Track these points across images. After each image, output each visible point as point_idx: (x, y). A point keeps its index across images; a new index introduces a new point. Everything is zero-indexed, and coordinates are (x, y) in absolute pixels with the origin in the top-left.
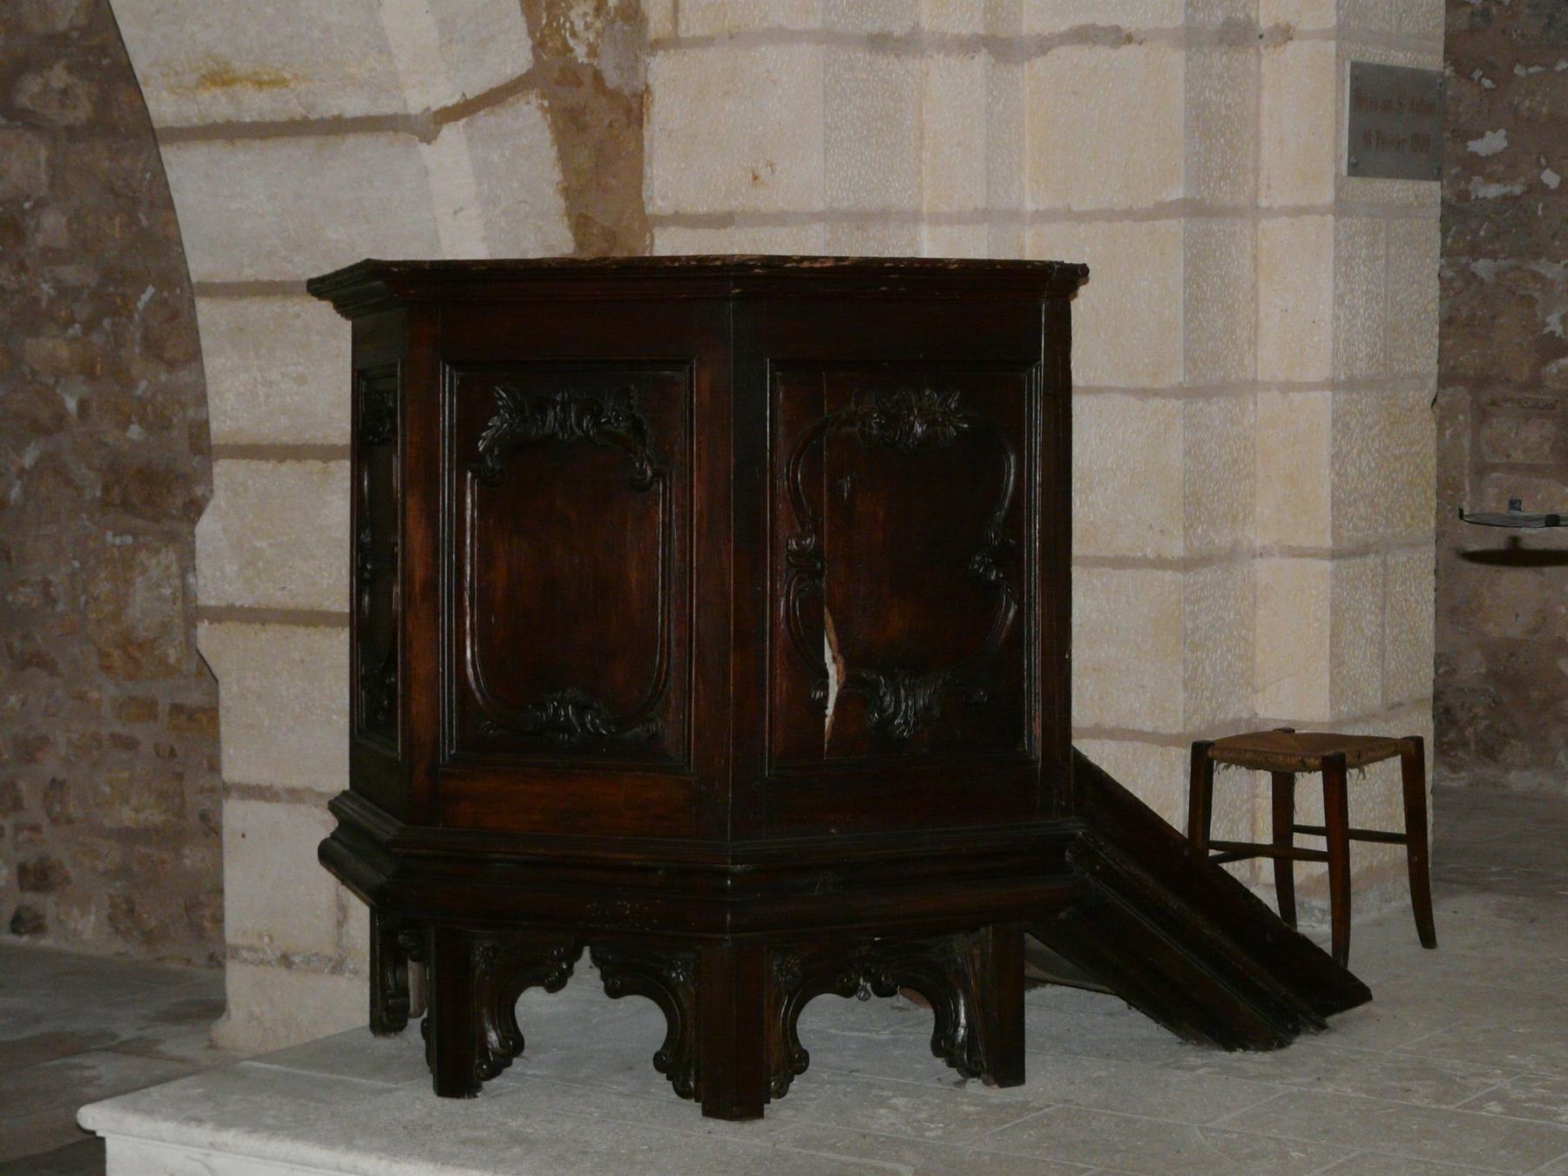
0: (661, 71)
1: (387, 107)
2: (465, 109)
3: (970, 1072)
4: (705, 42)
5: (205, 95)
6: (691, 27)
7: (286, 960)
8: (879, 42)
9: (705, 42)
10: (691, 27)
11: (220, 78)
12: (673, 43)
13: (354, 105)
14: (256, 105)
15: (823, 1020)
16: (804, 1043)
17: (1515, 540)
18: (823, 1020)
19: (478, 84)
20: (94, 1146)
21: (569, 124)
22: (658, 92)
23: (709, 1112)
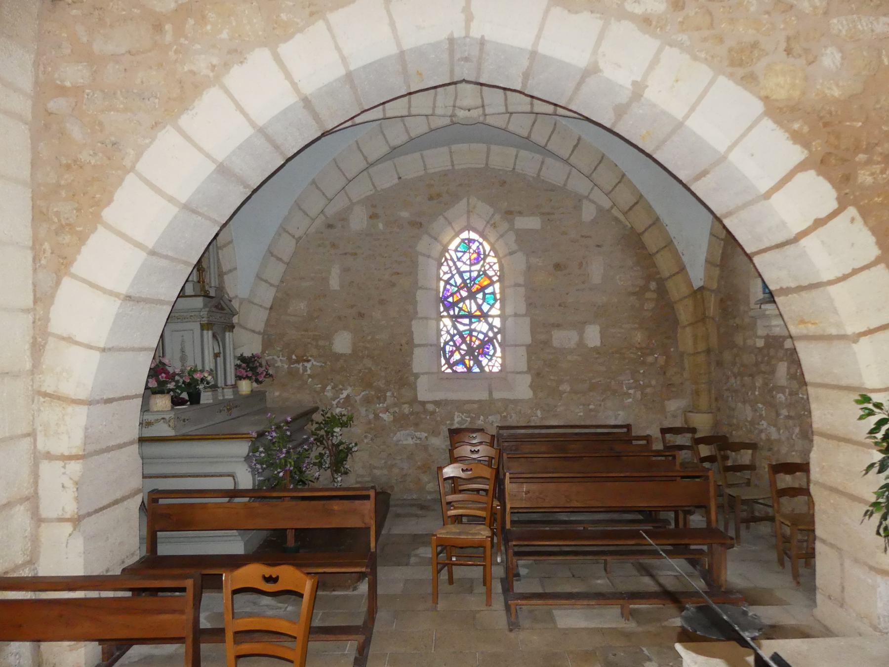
1: (842, 332)
5: (802, 326)
7: (829, 597)
13: (833, 331)
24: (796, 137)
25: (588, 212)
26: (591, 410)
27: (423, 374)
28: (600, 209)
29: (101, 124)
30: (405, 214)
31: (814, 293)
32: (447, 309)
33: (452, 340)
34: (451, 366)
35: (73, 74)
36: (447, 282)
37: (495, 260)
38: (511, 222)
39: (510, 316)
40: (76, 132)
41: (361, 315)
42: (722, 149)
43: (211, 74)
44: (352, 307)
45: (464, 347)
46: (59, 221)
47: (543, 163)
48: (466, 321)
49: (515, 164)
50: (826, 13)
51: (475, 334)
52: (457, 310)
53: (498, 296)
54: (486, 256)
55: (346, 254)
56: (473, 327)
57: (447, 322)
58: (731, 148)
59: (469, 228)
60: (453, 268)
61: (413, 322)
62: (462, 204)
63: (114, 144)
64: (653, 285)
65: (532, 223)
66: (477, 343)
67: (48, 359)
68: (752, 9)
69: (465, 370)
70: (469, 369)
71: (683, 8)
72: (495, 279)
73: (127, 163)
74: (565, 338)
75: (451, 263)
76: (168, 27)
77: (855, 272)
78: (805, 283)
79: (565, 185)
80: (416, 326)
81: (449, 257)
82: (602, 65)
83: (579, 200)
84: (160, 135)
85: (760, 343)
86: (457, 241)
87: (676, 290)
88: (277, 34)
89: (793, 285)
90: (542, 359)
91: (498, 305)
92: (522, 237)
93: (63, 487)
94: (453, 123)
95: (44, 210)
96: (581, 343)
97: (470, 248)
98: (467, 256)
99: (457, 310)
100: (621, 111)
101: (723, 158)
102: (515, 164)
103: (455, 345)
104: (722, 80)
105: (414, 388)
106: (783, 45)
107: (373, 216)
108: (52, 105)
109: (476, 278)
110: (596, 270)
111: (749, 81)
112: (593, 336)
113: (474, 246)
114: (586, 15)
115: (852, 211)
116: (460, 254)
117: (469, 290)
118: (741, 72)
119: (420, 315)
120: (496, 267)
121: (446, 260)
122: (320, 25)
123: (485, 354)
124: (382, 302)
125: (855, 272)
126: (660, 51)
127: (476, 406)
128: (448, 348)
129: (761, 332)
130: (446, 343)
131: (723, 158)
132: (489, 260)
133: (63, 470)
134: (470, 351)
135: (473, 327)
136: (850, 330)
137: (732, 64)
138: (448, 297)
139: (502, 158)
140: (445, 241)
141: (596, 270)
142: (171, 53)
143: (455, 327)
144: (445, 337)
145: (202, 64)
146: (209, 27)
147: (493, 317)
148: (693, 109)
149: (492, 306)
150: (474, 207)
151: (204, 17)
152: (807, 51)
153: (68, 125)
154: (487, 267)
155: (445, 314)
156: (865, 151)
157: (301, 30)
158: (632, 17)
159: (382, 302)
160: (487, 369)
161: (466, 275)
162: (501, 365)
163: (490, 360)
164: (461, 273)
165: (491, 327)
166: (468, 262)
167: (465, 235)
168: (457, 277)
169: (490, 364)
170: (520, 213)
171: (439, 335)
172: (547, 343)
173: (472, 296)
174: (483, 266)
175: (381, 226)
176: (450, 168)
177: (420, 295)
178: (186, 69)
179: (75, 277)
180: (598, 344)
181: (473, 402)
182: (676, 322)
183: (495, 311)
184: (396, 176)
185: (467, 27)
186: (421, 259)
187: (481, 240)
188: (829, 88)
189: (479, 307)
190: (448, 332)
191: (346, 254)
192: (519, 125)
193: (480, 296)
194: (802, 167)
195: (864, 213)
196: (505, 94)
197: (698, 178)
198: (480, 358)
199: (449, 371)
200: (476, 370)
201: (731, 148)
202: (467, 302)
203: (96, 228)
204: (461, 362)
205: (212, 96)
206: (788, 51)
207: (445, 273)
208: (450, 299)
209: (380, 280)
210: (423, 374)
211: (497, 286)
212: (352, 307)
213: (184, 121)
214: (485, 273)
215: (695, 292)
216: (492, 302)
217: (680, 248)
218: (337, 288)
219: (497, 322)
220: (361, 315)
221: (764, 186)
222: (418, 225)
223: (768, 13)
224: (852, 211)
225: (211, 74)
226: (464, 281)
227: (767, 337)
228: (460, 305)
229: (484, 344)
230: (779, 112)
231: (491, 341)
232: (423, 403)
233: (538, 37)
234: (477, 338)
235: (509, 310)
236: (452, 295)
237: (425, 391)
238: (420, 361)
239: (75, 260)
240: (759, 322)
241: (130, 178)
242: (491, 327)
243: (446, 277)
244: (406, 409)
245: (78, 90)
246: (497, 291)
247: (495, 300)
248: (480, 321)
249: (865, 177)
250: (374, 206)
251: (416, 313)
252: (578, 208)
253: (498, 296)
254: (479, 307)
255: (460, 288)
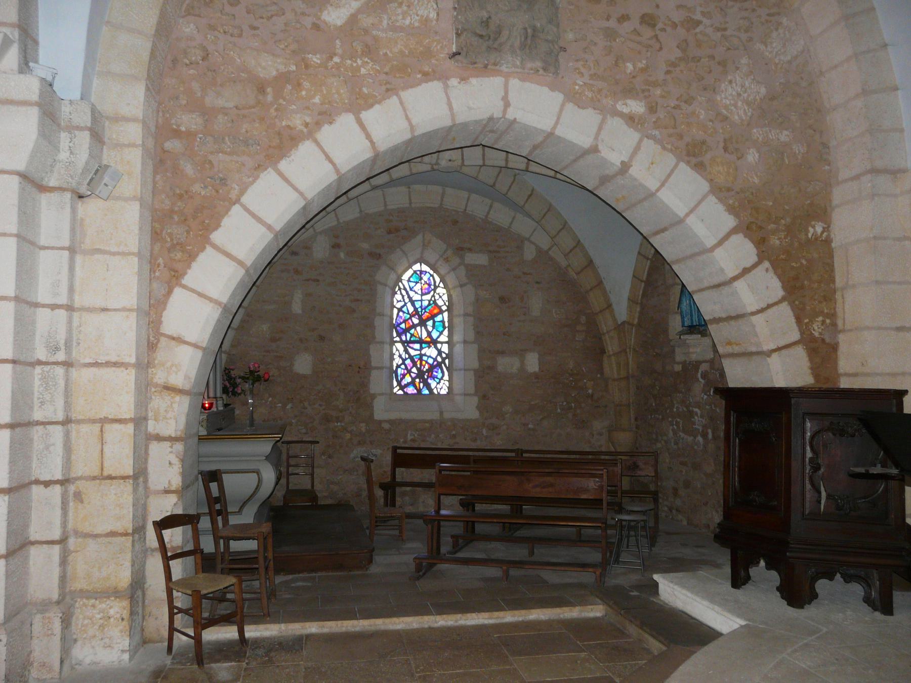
0: (841, 338)
1: (760, 350)
2: (779, 349)
3: (875, 609)
4: (851, 330)
5: (727, 347)
6: (848, 327)
8: (899, 329)
9: (851, 330)
10: (848, 327)
11: (729, 343)
12: (843, 331)
13: (754, 349)
14: (736, 349)
15: (822, 586)
16: (817, 590)
17: (867, 471)
18: (822, 586)
19: (782, 343)
20: (656, 585)
21: (812, 352)
22: (841, 344)
23: (789, 604)
24: (731, 210)
25: (529, 253)
26: (529, 429)
27: (380, 394)
28: (539, 251)
29: (210, 162)
30: (365, 246)
31: (740, 321)
32: (399, 335)
33: (403, 363)
34: (402, 388)
35: (189, 121)
36: (400, 310)
37: (444, 291)
38: (462, 258)
39: (458, 342)
40: (189, 169)
41: (322, 338)
42: (681, 214)
43: (305, 130)
44: (313, 330)
45: (414, 370)
46: (172, 240)
47: (491, 206)
48: (417, 346)
49: (466, 206)
50: (748, 125)
51: (425, 358)
52: (409, 335)
53: (447, 325)
54: (436, 287)
55: (308, 280)
56: (423, 352)
57: (400, 346)
58: (687, 215)
59: (421, 261)
60: (406, 297)
61: (371, 346)
62: (419, 238)
63: (221, 179)
64: (583, 319)
65: (481, 259)
66: (427, 367)
67: (160, 355)
68: (702, 117)
69: (415, 391)
70: (419, 391)
71: (656, 112)
72: (444, 308)
73: (233, 195)
74: (507, 364)
75: (404, 292)
76: (269, 90)
77: (769, 306)
78: (733, 314)
79: (510, 227)
80: (373, 350)
81: (402, 287)
82: (600, 147)
83: (520, 242)
84: (262, 175)
85: (678, 368)
86: (410, 272)
87: (605, 324)
88: (359, 103)
89: (724, 315)
90: (485, 380)
91: (446, 332)
92: (471, 270)
93: (170, 463)
94: (433, 170)
95: (159, 231)
96: (522, 369)
97: (421, 279)
98: (419, 286)
99: (409, 335)
100: (605, 180)
101: (681, 221)
102: (466, 206)
103: (406, 368)
104: (682, 165)
105: (370, 407)
106: (722, 145)
107: (336, 246)
108: (168, 145)
109: (426, 307)
110: (536, 303)
111: (699, 167)
112: (532, 363)
113: (425, 278)
114: (590, 111)
115: (766, 264)
116: (412, 284)
117: (420, 318)
118: (694, 160)
119: (377, 340)
120: (445, 298)
121: (400, 289)
122: (394, 99)
123: (434, 378)
124: (341, 326)
125: (769, 306)
126: (641, 141)
127: (427, 425)
128: (400, 371)
129: (679, 357)
130: (398, 366)
131: (681, 221)
132: (439, 290)
133: (170, 449)
134: (420, 374)
135: (423, 352)
136: (766, 348)
137: (688, 155)
138: (401, 323)
139: (455, 200)
140: (400, 271)
141: (536, 303)
142: (272, 111)
143: (406, 351)
144: (397, 361)
145: (297, 121)
146: (304, 93)
147: (442, 343)
148: (663, 185)
149: (441, 333)
150: (429, 242)
151: (299, 85)
152: (737, 150)
153: (182, 162)
154: (437, 297)
155: (398, 339)
156: (774, 223)
157: (379, 102)
158: (621, 115)
159: (341, 326)
160: (435, 391)
161: (418, 305)
162: (449, 388)
163: (438, 383)
164: (413, 302)
165: (440, 352)
166: (420, 292)
167: (417, 267)
168: (409, 305)
169: (439, 386)
170: (470, 250)
171: (392, 359)
172: (492, 368)
173: (423, 323)
174: (433, 296)
175: (342, 255)
176: (408, 205)
177: (377, 321)
178: (284, 123)
179: (184, 287)
180: (537, 369)
181: (425, 421)
182: (603, 351)
183: (444, 338)
184: (358, 210)
185: (505, 112)
186: (380, 288)
187: (432, 272)
188: (752, 177)
189: (429, 334)
190: (400, 356)
191: (308, 280)
192: (487, 176)
193: (430, 323)
194: (734, 231)
195: (775, 266)
196: (484, 150)
197: (657, 233)
198: (430, 381)
199: (401, 392)
200: (426, 392)
201: (687, 215)
202: (418, 328)
203: (205, 248)
204: (412, 383)
205: (306, 148)
206: (725, 149)
207: (398, 301)
208: (403, 326)
209: (340, 306)
210: (380, 394)
211: (446, 314)
212: (313, 330)
213: (283, 165)
214: (435, 302)
215: (619, 325)
216: (441, 329)
217: (608, 289)
218: (300, 312)
219: (445, 348)
220: (322, 338)
221: (710, 242)
222: (376, 256)
223: (711, 121)
224: (766, 264)
225: (305, 130)
226: (416, 309)
227: (684, 364)
228: (412, 331)
229: (432, 368)
230: (718, 190)
231: (439, 365)
232: (380, 422)
233: (557, 123)
234: (427, 362)
235: (457, 338)
236: (405, 321)
237: (381, 411)
238: (376, 384)
239: (185, 274)
240: (677, 350)
241: (236, 209)
242: (440, 352)
243: (399, 305)
244: (363, 427)
245: (190, 135)
246: (446, 320)
247: (444, 327)
248: (429, 347)
249: (775, 241)
250: (337, 237)
251: (374, 338)
252: (520, 248)
253: (447, 325)
254: (429, 334)
255: (412, 316)
